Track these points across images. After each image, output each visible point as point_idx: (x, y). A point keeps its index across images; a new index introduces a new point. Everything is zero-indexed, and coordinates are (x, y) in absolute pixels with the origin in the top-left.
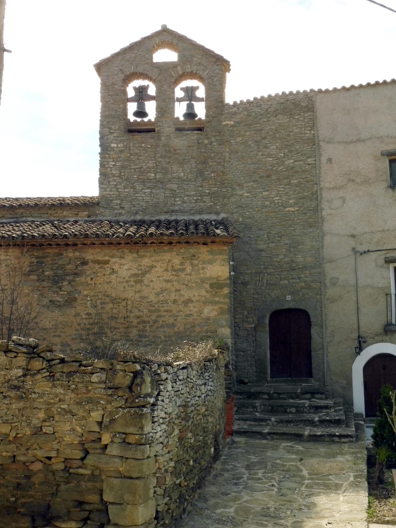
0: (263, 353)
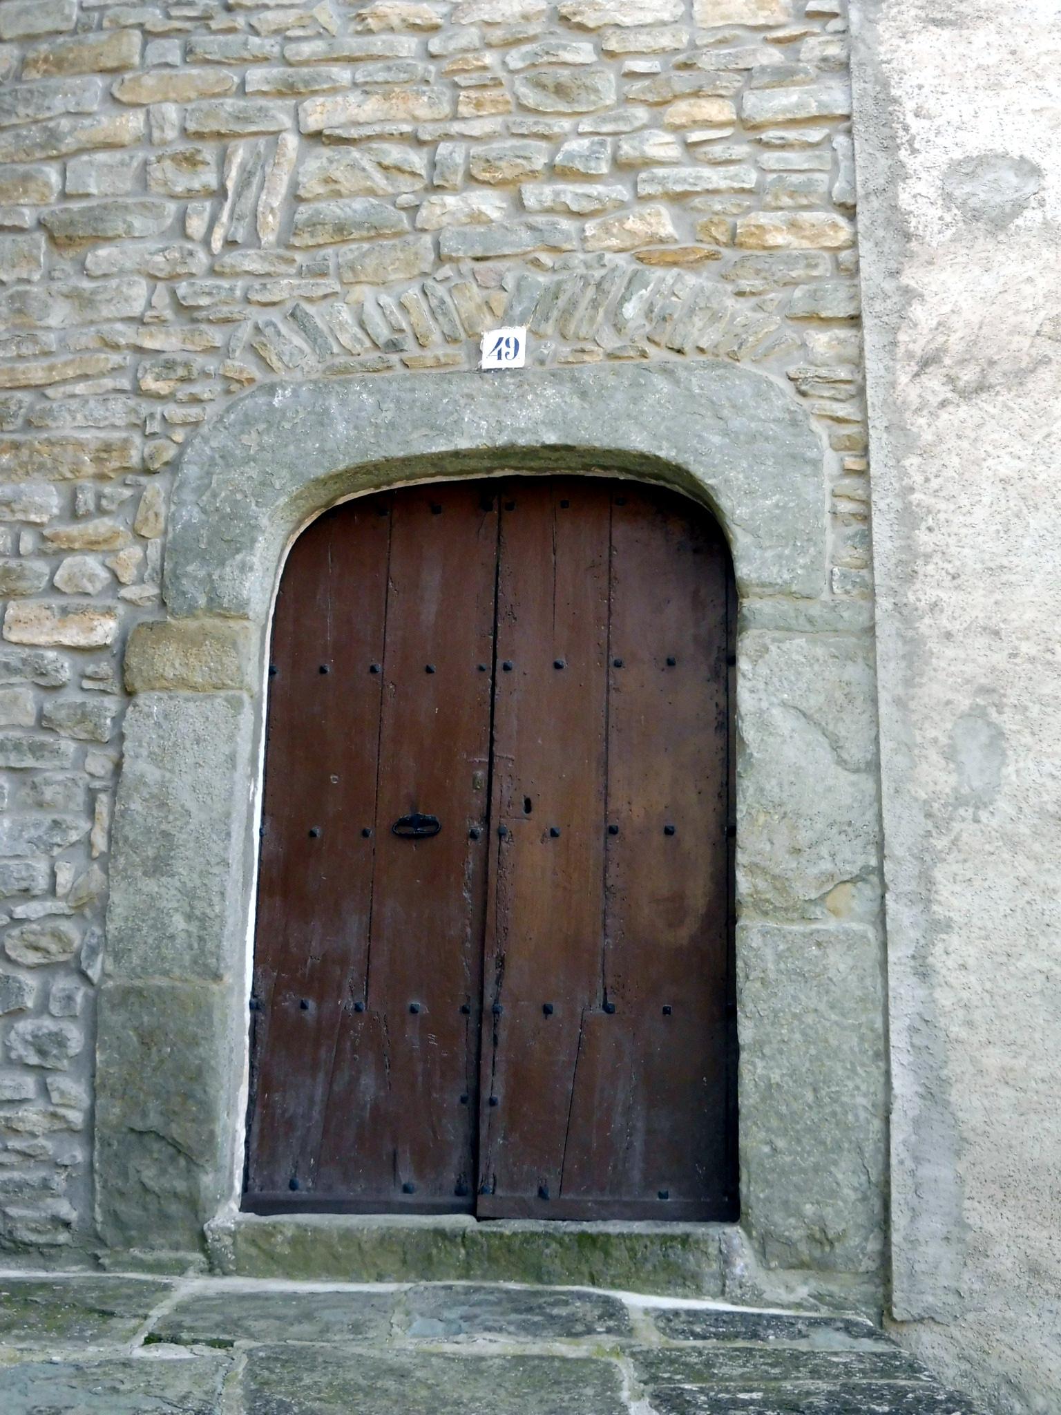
0: (178, 923)
